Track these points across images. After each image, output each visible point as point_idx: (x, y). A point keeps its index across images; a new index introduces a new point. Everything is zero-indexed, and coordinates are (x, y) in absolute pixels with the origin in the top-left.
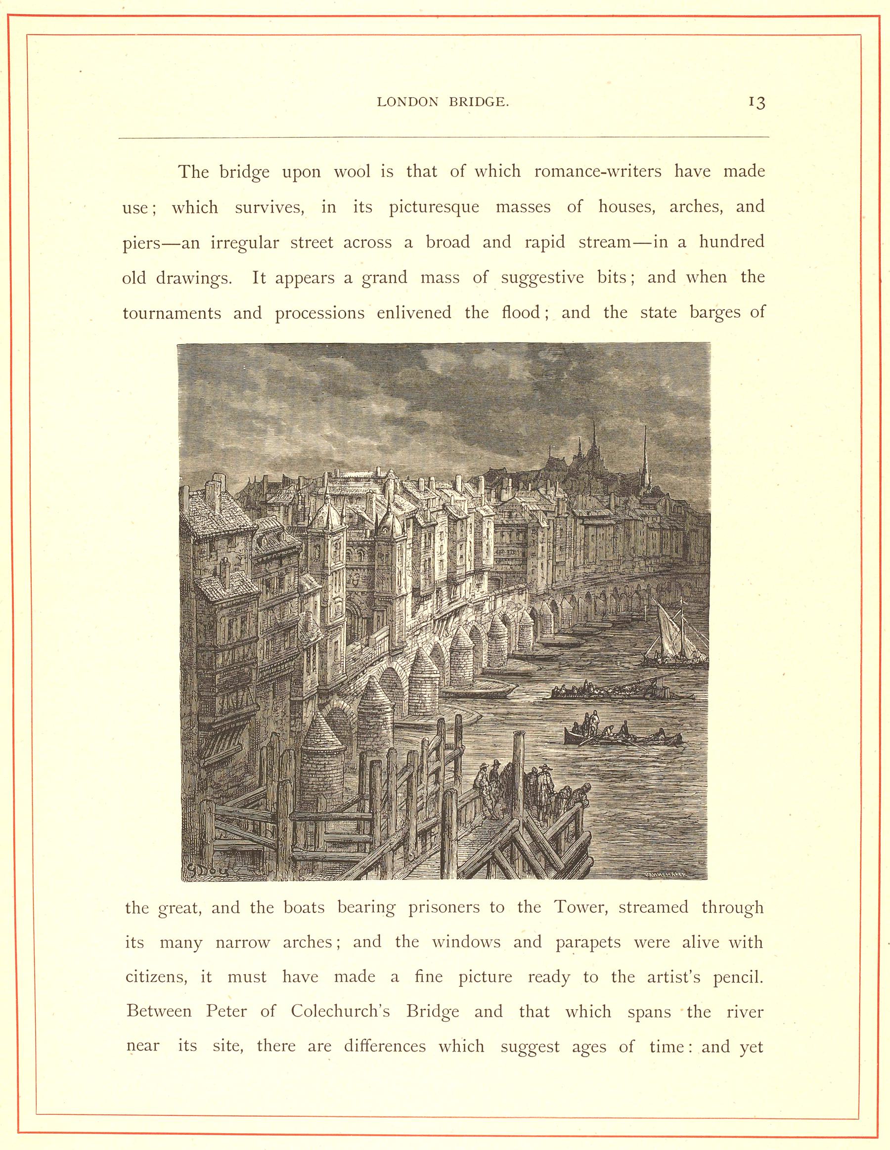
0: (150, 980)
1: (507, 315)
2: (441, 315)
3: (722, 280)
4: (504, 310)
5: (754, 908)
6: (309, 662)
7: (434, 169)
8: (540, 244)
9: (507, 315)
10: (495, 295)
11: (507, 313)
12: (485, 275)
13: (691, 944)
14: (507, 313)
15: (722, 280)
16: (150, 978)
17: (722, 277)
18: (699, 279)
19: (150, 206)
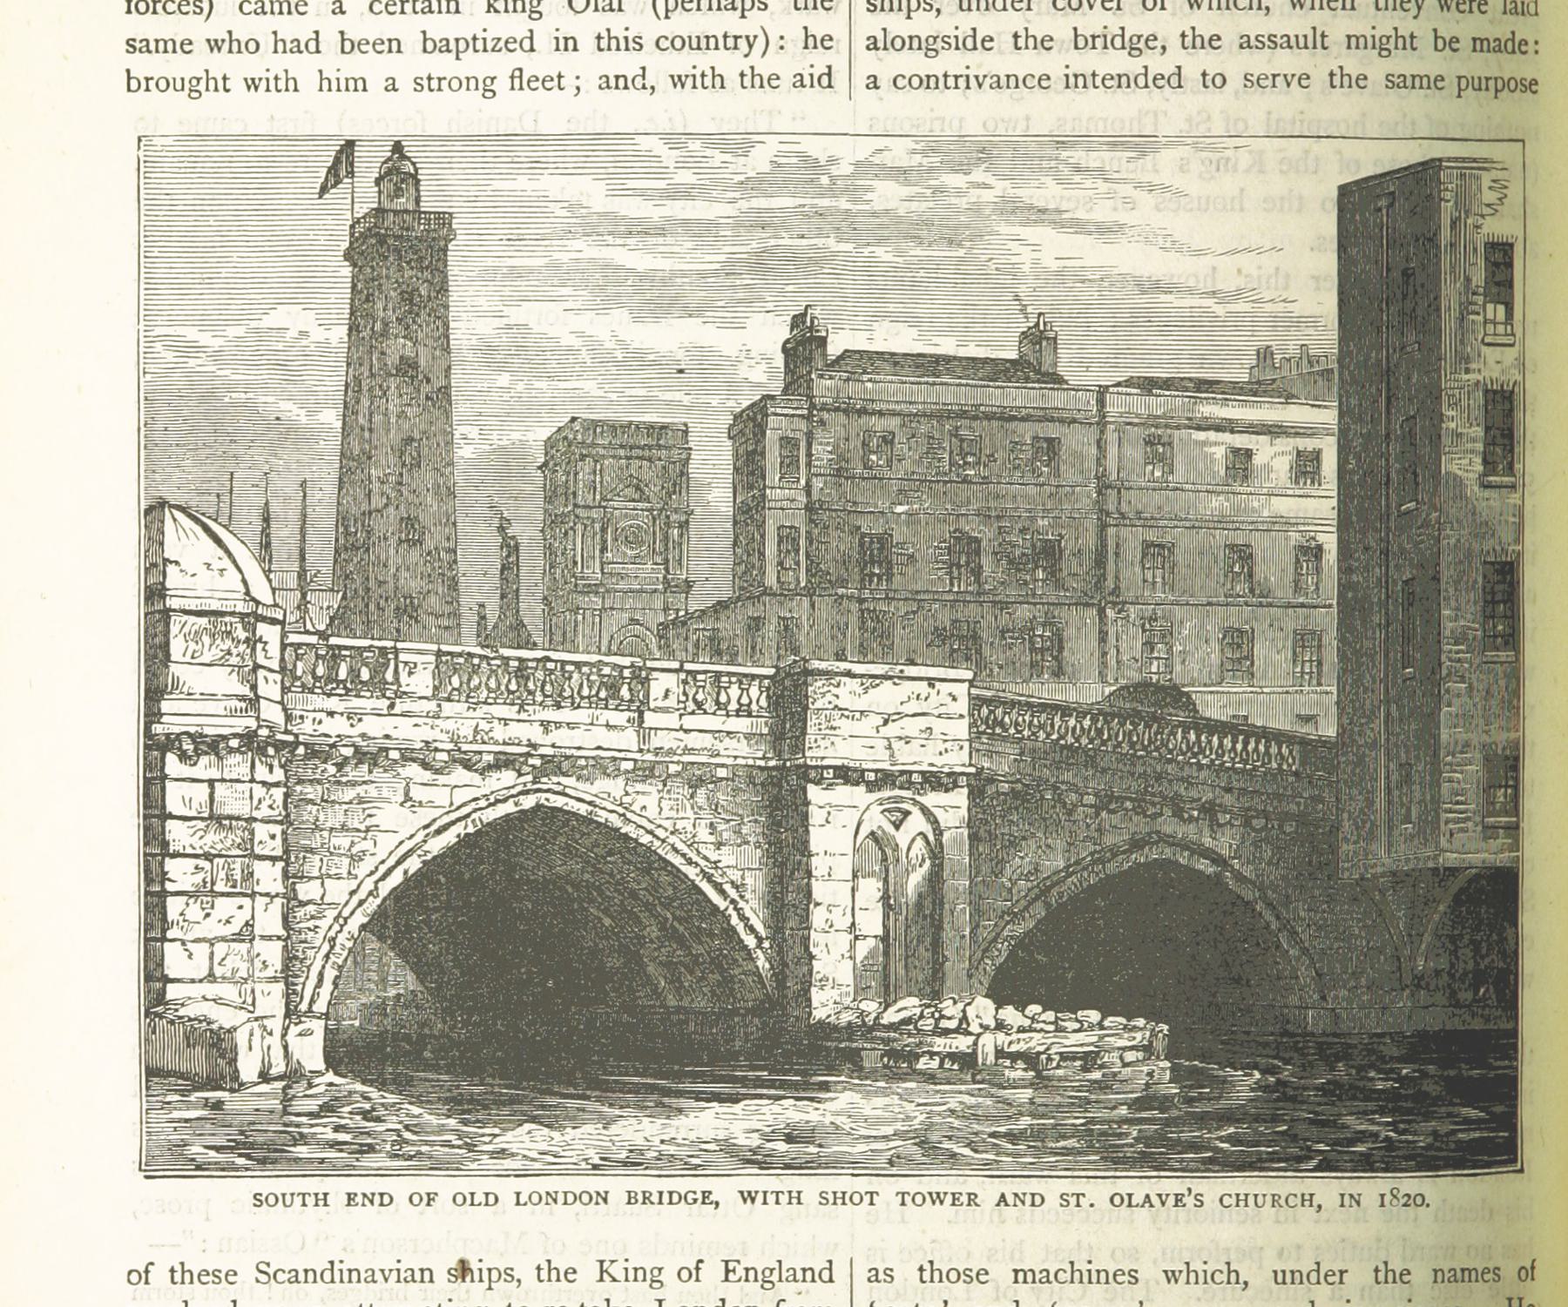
0: (489, 47)
1: (517, 85)
2: (517, 46)
3: (395, 48)
4: (512, 77)
5: (1392, 40)
6: (929, 46)
7: (225, 78)
8: (452, 46)
9: (517, 85)
10: (764, 1110)
11: (517, 81)
12: (698, 1269)
13: (880, 44)
14: (517, 81)
15: (395, 48)
16: (490, 46)
17: (394, 44)
18: (226, 47)
19: (1531, 43)
